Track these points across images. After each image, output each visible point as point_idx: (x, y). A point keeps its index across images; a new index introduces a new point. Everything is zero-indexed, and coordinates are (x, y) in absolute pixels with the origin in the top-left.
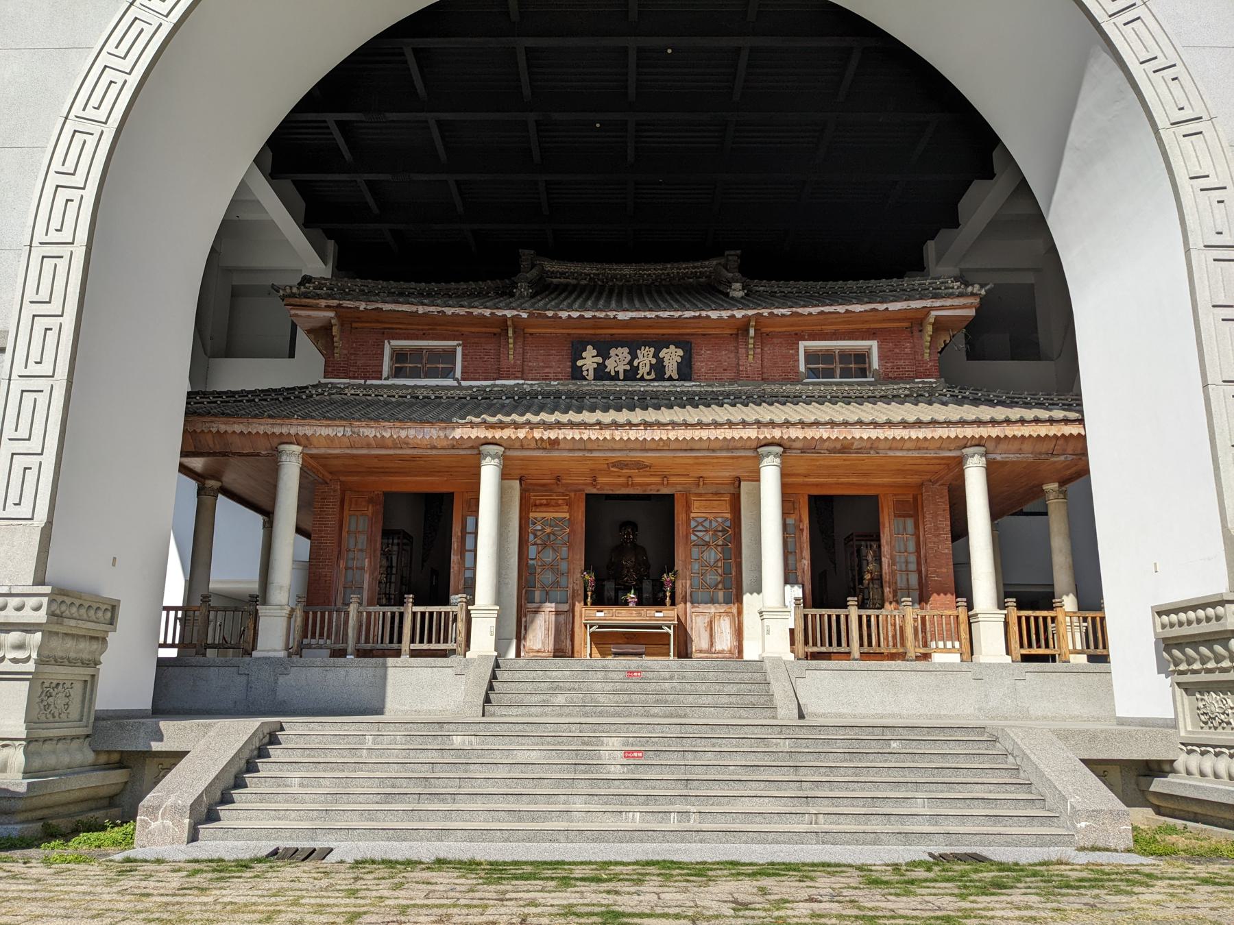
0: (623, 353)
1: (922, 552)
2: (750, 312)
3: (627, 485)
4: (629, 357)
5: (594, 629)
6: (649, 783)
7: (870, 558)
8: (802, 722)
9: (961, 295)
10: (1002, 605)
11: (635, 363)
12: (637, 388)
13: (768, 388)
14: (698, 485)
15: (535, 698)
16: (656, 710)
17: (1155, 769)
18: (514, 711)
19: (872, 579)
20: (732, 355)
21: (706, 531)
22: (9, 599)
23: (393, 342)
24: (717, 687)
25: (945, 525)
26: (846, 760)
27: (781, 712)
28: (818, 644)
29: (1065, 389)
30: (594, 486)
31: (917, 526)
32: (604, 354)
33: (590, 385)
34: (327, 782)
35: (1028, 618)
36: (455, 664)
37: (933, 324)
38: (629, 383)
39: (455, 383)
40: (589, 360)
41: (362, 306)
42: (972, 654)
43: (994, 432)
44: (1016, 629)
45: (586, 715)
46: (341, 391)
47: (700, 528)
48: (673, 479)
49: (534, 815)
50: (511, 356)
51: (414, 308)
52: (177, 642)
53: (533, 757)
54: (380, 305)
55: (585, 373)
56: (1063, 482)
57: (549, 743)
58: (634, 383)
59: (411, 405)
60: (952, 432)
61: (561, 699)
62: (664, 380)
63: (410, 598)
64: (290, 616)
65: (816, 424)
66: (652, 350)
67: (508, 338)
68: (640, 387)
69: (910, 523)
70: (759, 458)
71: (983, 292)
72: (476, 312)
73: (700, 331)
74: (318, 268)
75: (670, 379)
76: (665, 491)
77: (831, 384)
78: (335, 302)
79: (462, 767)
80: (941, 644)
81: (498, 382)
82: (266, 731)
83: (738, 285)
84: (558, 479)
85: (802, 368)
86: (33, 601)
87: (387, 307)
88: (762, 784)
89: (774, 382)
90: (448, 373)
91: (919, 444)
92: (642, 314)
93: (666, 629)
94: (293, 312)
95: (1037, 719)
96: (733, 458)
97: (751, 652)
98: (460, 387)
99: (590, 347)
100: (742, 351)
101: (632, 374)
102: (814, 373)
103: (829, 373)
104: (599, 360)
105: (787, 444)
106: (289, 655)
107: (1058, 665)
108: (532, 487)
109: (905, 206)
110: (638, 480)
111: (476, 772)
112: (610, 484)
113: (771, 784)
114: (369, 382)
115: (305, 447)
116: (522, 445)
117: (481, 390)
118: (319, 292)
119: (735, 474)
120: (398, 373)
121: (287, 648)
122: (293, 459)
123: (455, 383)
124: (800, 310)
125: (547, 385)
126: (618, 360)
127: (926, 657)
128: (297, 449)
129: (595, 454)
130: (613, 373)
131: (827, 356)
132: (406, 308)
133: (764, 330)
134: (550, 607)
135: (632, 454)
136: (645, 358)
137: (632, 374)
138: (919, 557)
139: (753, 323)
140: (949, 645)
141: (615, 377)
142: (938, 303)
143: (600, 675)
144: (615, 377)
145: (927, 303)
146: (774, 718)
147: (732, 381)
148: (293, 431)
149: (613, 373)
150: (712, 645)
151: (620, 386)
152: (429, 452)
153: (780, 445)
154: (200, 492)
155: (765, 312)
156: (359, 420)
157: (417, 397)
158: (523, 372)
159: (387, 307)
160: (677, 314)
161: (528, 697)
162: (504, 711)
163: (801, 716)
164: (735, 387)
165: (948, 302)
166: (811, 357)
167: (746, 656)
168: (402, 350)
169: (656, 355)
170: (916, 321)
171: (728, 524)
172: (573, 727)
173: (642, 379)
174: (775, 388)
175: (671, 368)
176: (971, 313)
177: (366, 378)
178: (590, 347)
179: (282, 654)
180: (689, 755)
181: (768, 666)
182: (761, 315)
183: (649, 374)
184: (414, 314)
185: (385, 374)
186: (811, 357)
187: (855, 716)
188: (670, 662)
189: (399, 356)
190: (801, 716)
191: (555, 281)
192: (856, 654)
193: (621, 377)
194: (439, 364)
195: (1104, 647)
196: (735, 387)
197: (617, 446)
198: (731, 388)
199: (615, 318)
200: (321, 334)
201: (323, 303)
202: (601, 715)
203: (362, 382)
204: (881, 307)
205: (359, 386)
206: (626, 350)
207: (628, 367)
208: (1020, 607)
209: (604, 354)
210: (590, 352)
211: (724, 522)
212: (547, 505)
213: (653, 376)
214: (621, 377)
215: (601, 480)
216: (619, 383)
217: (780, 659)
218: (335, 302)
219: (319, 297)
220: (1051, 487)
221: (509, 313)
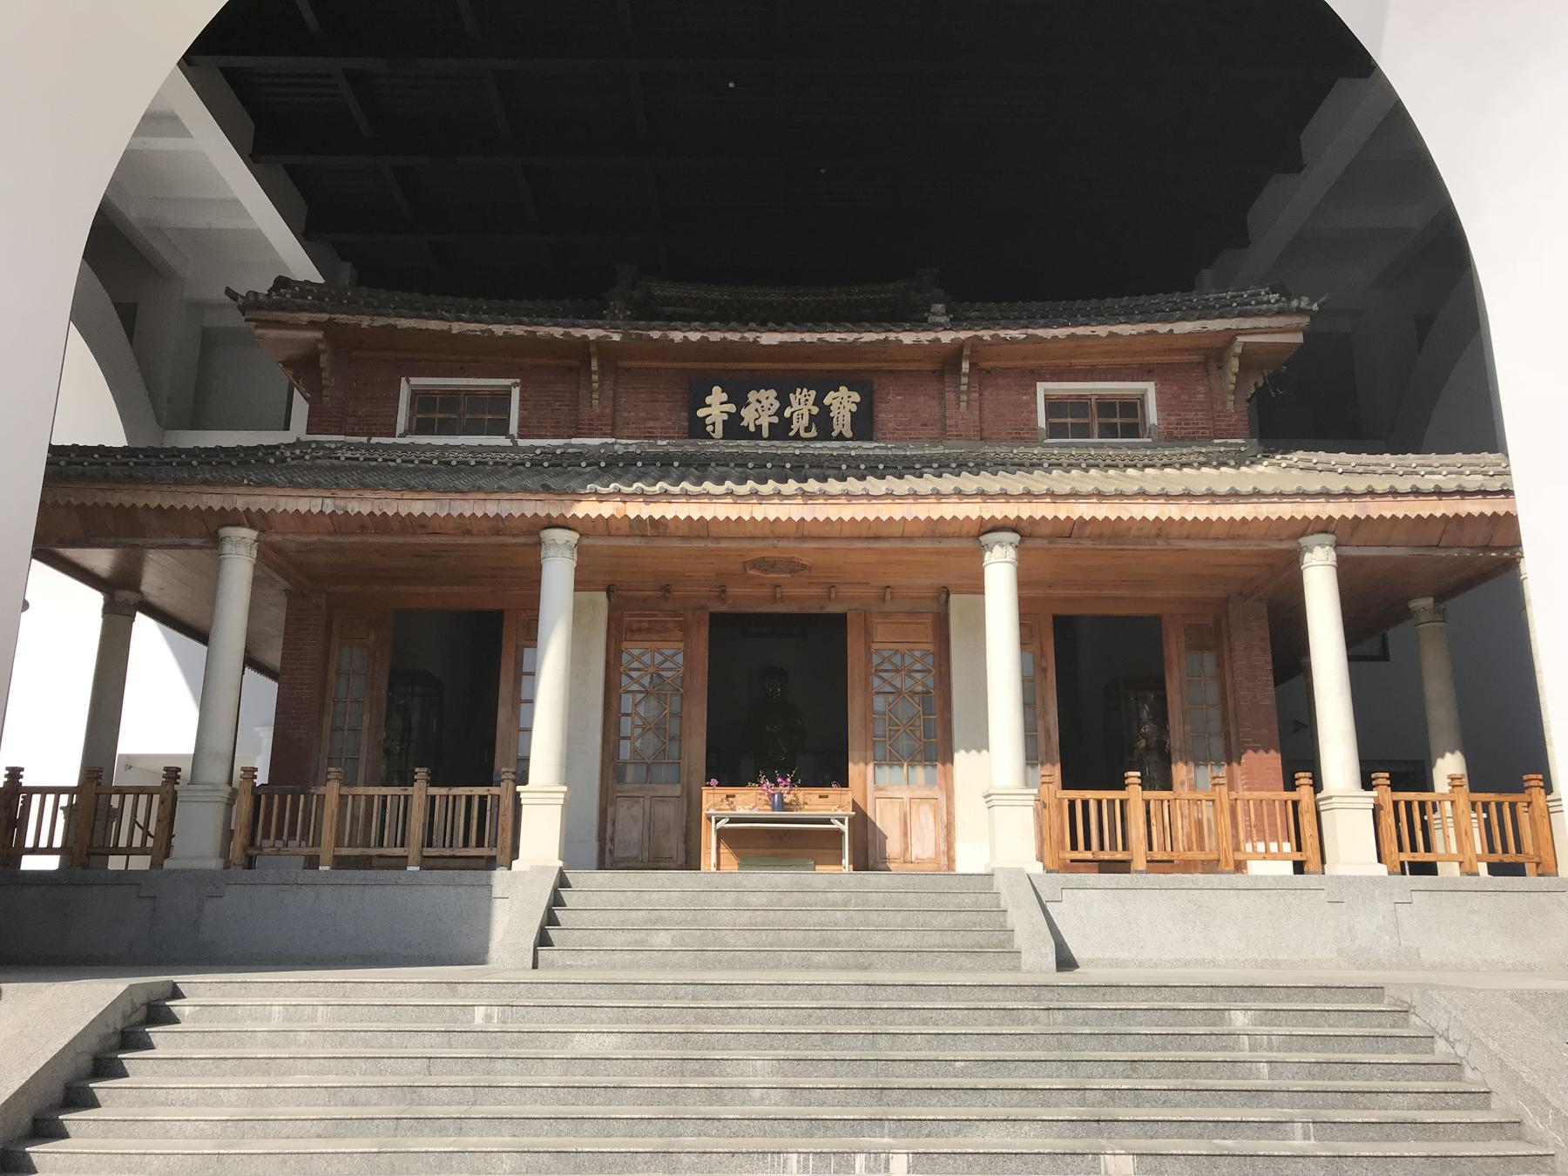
0: (768, 397)
1: (1230, 703)
2: (963, 335)
3: (774, 599)
4: (777, 405)
5: (722, 824)
6: (814, 1095)
7: (1145, 715)
8: (1066, 978)
9: (1280, 313)
10: (1367, 784)
11: (787, 413)
12: (789, 451)
13: (990, 451)
14: (884, 599)
15: (621, 938)
16: (822, 957)
18: (586, 958)
19: (1147, 748)
20: (935, 403)
21: (897, 671)
23: (414, 381)
24: (921, 917)
25: (1264, 661)
26: (1155, 1048)
27: (1027, 960)
28: (1086, 848)
29: (1480, 429)
30: (723, 600)
31: (1220, 665)
32: (739, 399)
33: (718, 444)
34: (232, 1096)
35: (1409, 804)
37: (1241, 357)
38: (777, 443)
39: (508, 442)
40: (716, 407)
41: (366, 322)
42: (1323, 862)
43: (1349, 510)
44: (1391, 820)
45: (705, 966)
46: (331, 453)
47: (886, 666)
48: (846, 591)
49: (885, 1050)
50: (596, 404)
51: (443, 325)
52: (57, 843)
53: (607, 1045)
54: (392, 321)
55: (709, 429)
56: (1441, 596)
57: (638, 1020)
58: (786, 444)
59: (434, 471)
60: (1285, 510)
61: (662, 939)
62: (831, 439)
63: (421, 773)
64: (230, 803)
65: (1075, 495)
66: (813, 393)
67: (591, 373)
68: (796, 448)
69: (1209, 660)
70: (978, 553)
71: (1315, 307)
72: (542, 331)
73: (886, 366)
74: (301, 266)
75: (841, 437)
77: (1087, 446)
78: (325, 317)
79: (483, 1065)
80: (1261, 847)
81: (574, 441)
82: (140, 999)
83: (939, 307)
84: (666, 589)
85: (1042, 422)
87: (404, 323)
88: (1016, 1096)
89: (999, 441)
90: (501, 428)
91: (1161, 528)
92: (797, 337)
93: (837, 825)
94: (259, 331)
95: (1433, 967)
96: (938, 553)
97: (969, 860)
98: (515, 448)
99: (716, 389)
100: (950, 396)
101: (781, 429)
102: (1055, 430)
103: (1082, 431)
104: (732, 408)
105: (1028, 530)
106: (227, 866)
107: (1530, 880)
108: (633, 594)
110: (789, 591)
111: (510, 1077)
112: (748, 597)
113: (1032, 1096)
114: (374, 440)
115: (262, 531)
117: (549, 453)
118: (299, 301)
119: (943, 582)
120: (421, 426)
121: (225, 852)
122: (242, 550)
123: (508, 442)
124: (1041, 332)
125: (651, 445)
126: (761, 408)
127: (1240, 867)
128: (249, 534)
129: (725, 544)
130: (752, 429)
131: (1079, 405)
132: (433, 325)
133: (984, 365)
134: (258, 782)
135: (783, 544)
136: (802, 405)
137: (781, 429)
138: (1225, 711)
139: (966, 352)
140: (1273, 847)
141: (757, 435)
142: (1247, 323)
143: (730, 898)
144: (757, 435)
145: (1233, 323)
146: (1017, 969)
147: (935, 441)
148: (240, 503)
149: (752, 429)
150: (906, 849)
151: (763, 447)
152: (460, 540)
153: (1015, 531)
154: (109, 610)
155: (986, 335)
156: (347, 489)
157: (449, 463)
158: (614, 426)
159: (404, 323)
160: (850, 337)
161: (610, 935)
162: (569, 959)
163: (1065, 961)
164: (940, 450)
165: (1263, 322)
166: (1054, 406)
167: (961, 867)
168: (427, 392)
169: (818, 402)
170: (1212, 354)
171: (930, 660)
172: (682, 990)
173: (797, 437)
174: (1002, 450)
176: (1298, 338)
177: (370, 435)
178: (716, 389)
179: (214, 864)
180: (883, 1042)
181: (999, 883)
182: (980, 339)
183: (808, 430)
184: (446, 335)
185: (400, 428)
186: (1054, 406)
187: (1140, 965)
188: (836, 876)
189: (421, 399)
190: (1065, 961)
192: (1140, 863)
193: (765, 433)
194: (486, 413)
195: (1125, 848)
196: (940, 450)
197: (758, 533)
198: (934, 451)
199: (755, 341)
200: (304, 368)
201: (305, 317)
202: (729, 966)
203: (364, 439)
204: (1163, 328)
205: (358, 446)
206: (772, 393)
207: (775, 420)
208: (1395, 787)
209: (739, 399)
210: (717, 396)
211: (922, 658)
212: (649, 630)
213: (814, 433)
214: (765, 433)
215: (733, 591)
216: (762, 443)
217: (1021, 870)
218: (325, 317)
219: (301, 309)
220: (1424, 603)
221: (592, 334)
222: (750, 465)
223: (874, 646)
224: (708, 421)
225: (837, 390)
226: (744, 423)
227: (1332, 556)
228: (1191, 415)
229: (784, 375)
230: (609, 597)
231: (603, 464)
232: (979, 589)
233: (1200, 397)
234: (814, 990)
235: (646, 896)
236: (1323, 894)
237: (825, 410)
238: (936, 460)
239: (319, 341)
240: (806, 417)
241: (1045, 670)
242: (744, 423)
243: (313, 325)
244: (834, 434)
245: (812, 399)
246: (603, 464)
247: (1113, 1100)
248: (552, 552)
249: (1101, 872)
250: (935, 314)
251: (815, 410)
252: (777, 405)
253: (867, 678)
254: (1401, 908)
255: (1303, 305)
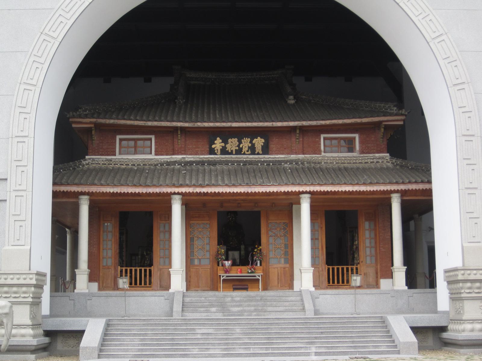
5: (224, 278)
9: (396, 115)
11: (241, 146)
17: (443, 329)
22: (21, 276)
32: (225, 141)
33: (218, 157)
36: (165, 295)
40: (218, 144)
55: (216, 151)
66: (249, 139)
75: (258, 154)
76: (256, 209)
86: (31, 276)
93: (259, 277)
99: (218, 138)
104: (223, 144)
108: (194, 208)
109: (368, 81)
116: (190, 194)
130: (230, 151)
136: (246, 143)
144: (231, 153)
149: (230, 151)
169: (251, 142)
173: (244, 154)
175: (259, 148)
178: (218, 138)
183: (248, 151)
190: (30, 270)
191: (192, 82)
193: (234, 153)
206: (236, 139)
207: (237, 148)
209: (225, 141)
214: (234, 153)
217: (308, 290)
222: (230, 164)
223: (269, 221)
224: (216, 149)
225: (257, 138)
226: (227, 149)
227: (399, 200)
228: (369, 145)
229: (240, 133)
230: (186, 207)
231: (183, 165)
232: (299, 203)
233: (373, 139)
234: (254, 320)
235: (207, 298)
236: (389, 295)
237: (253, 145)
238: (289, 162)
239: (93, 127)
240: (247, 147)
241: (322, 228)
242: (227, 149)
243: (91, 123)
244: (256, 152)
245: (249, 141)
246: (183, 165)
247: (316, 339)
248: (175, 202)
249: (235, 289)
250: (290, 100)
251: (250, 145)
252: (238, 143)
253: (267, 232)
254: (410, 298)
255: (403, 112)
